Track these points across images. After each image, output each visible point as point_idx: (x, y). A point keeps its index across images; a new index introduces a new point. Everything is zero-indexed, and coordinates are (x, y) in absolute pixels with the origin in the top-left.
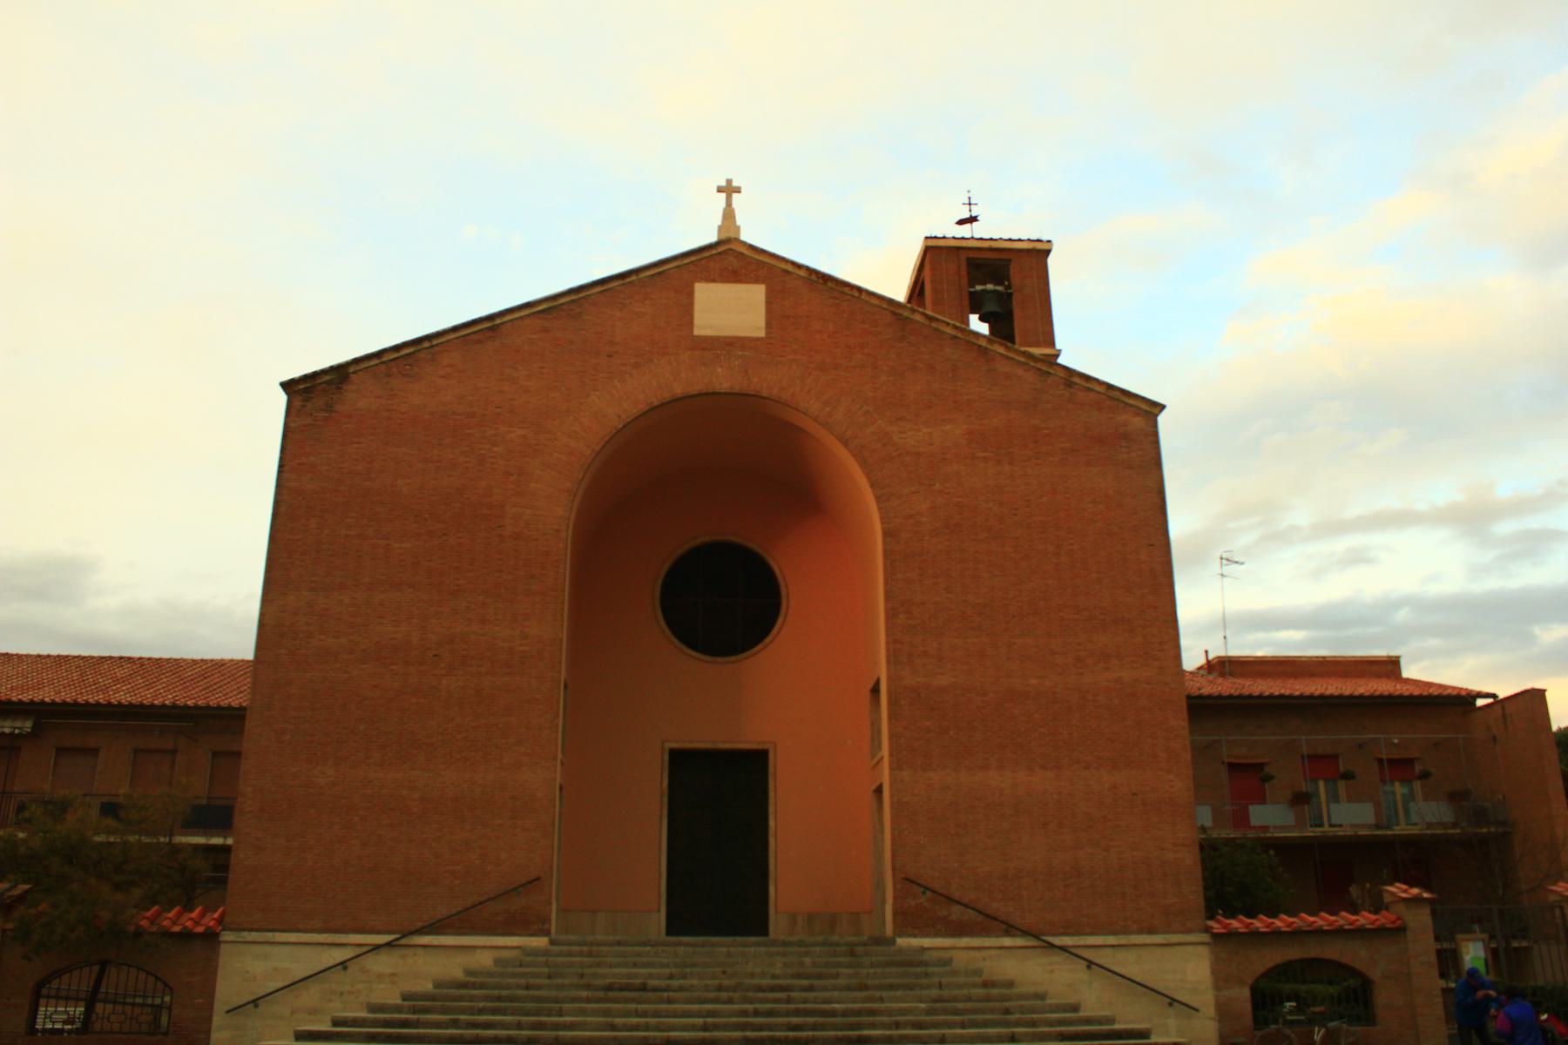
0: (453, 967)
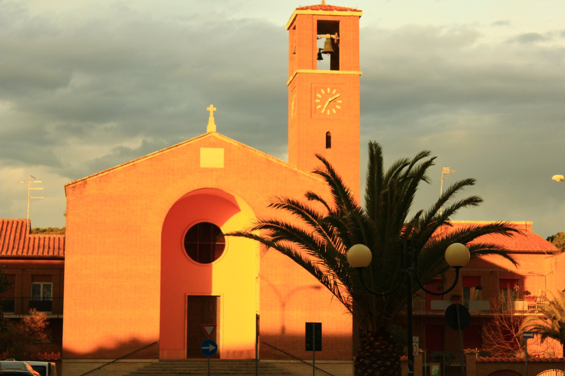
0: (133, 369)
